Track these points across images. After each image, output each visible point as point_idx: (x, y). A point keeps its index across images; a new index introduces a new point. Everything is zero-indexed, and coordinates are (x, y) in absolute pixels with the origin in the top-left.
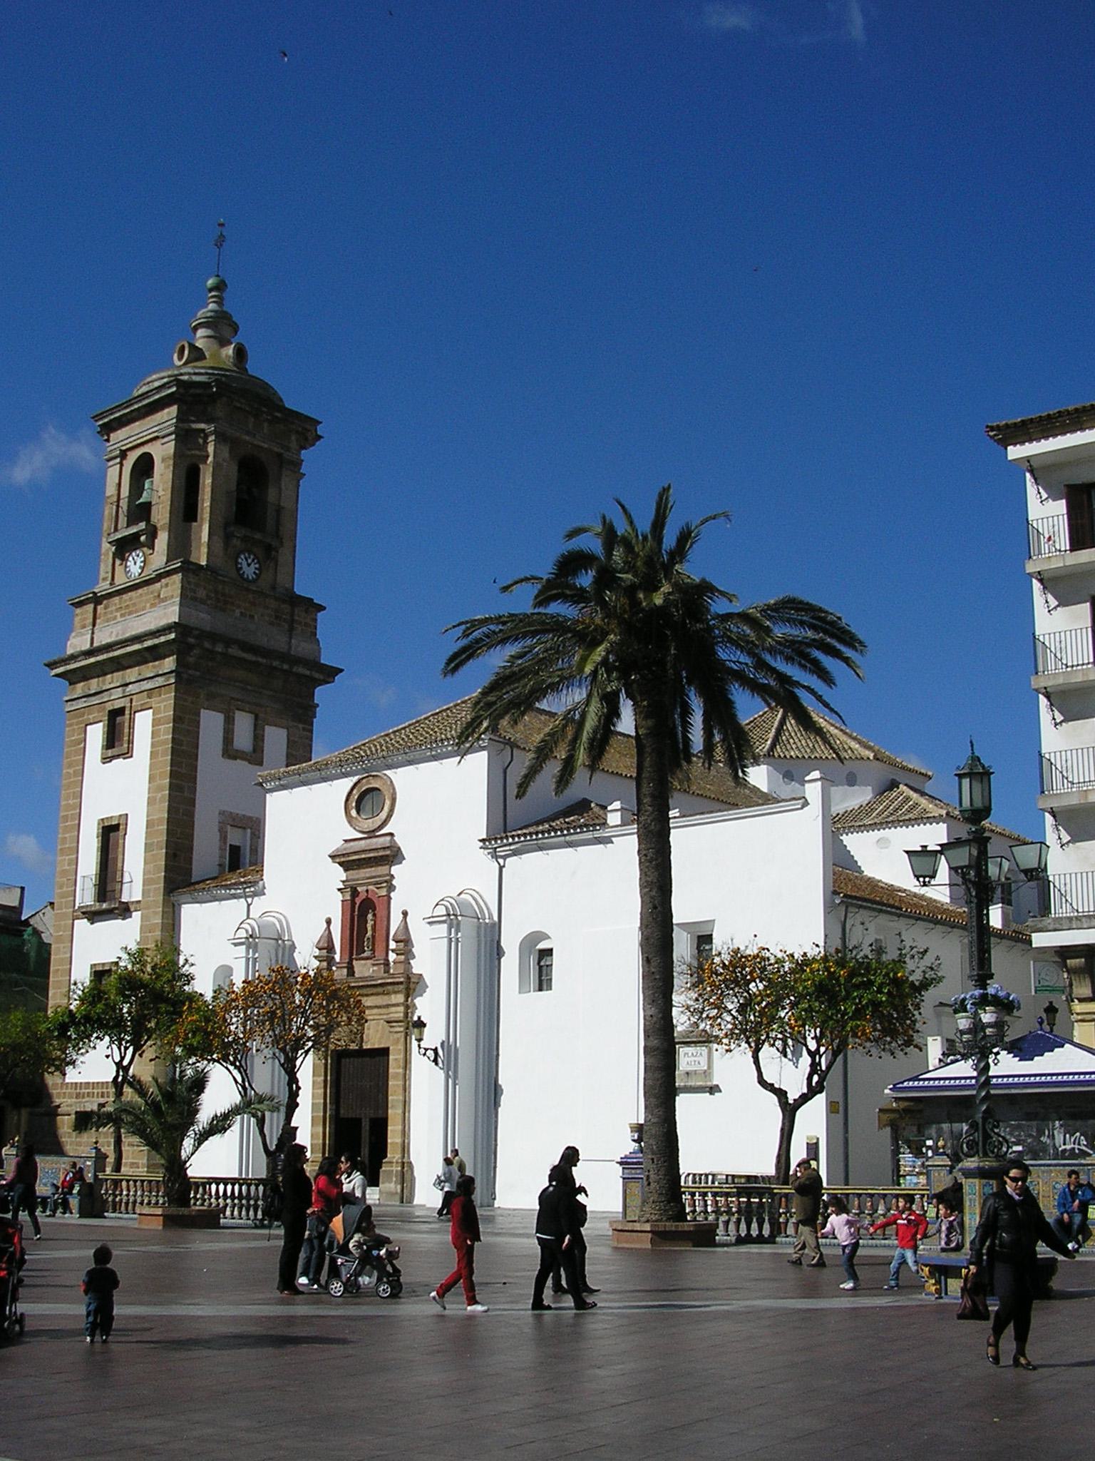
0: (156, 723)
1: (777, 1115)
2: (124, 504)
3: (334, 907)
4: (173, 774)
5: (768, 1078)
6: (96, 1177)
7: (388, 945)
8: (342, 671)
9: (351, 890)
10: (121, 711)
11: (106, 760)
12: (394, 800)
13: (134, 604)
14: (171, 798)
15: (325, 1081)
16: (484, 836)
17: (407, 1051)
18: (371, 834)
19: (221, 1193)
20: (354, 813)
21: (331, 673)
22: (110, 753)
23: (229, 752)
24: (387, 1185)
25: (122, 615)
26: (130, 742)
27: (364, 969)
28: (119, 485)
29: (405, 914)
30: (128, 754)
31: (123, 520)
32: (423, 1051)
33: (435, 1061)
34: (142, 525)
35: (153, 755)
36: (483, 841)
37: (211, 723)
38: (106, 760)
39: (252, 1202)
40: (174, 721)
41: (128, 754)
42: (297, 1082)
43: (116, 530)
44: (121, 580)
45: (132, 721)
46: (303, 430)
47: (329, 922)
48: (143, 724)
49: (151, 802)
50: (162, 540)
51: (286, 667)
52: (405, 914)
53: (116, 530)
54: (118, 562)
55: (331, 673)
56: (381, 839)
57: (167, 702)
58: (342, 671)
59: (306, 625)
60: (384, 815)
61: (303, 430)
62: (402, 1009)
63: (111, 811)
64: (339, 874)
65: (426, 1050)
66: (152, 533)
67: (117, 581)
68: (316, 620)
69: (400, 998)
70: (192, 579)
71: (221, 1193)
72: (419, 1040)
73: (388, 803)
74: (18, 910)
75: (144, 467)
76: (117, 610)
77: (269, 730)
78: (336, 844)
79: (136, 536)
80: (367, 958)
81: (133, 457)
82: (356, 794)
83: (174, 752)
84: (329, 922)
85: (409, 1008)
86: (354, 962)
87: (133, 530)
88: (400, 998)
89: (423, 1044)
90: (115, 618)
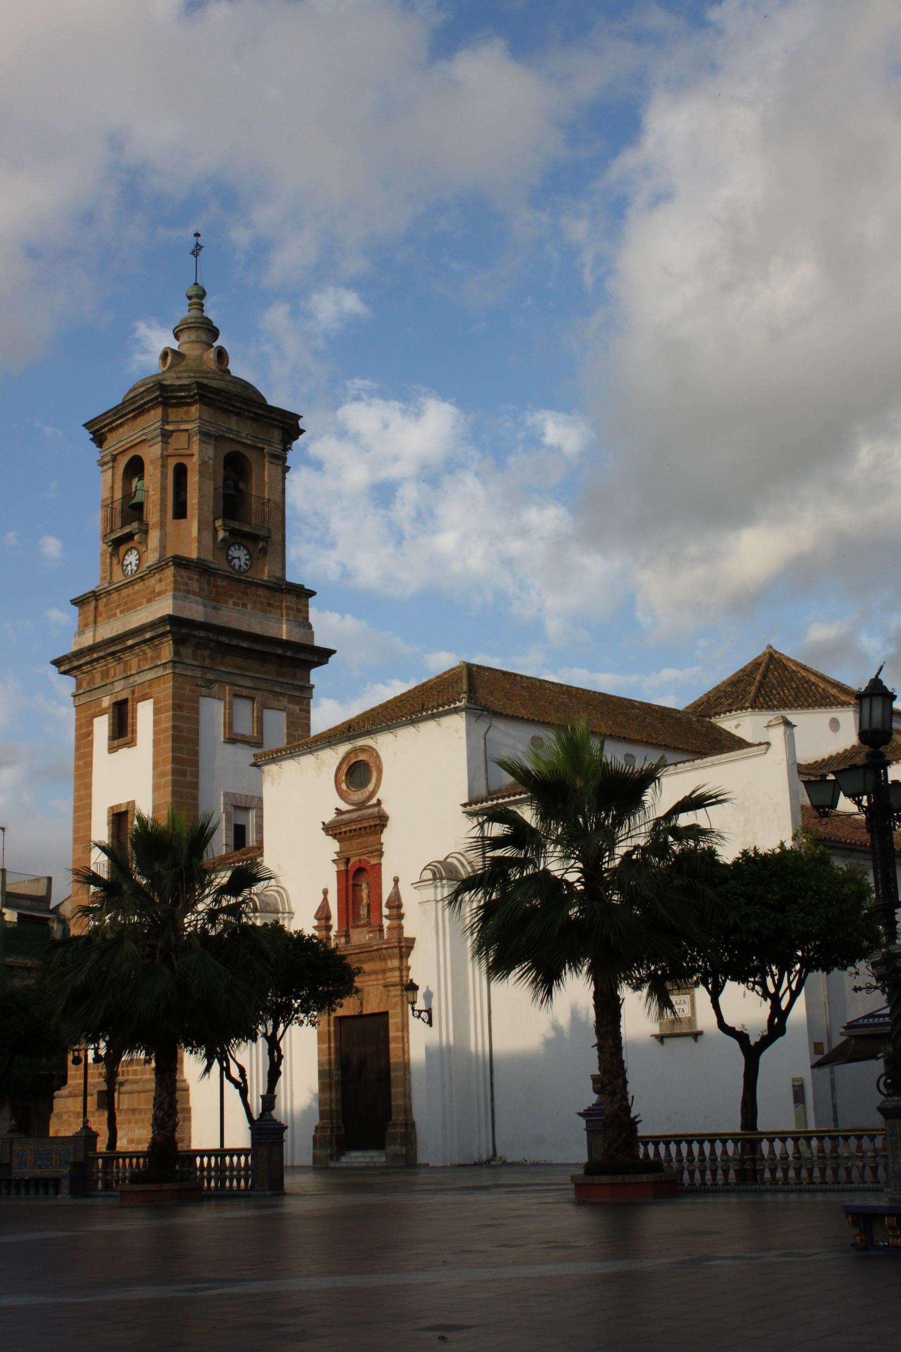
0: (157, 711)
1: (739, 1060)
2: (118, 506)
3: (328, 878)
4: (175, 760)
5: (729, 1021)
6: (86, 1155)
7: (381, 913)
8: (334, 652)
9: (343, 859)
10: (125, 701)
11: (112, 749)
12: (380, 771)
13: (132, 601)
14: (174, 783)
15: (329, 1048)
16: (466, 801)
17: (404, 1016)
18: (361, 805)
19: (205, 1164)
20: (344, 786)
21: (323, 655)
22: (116, 743)
23: (233, 739)
24: (392, 1147)
25: (121, 612)
26: (134, 731)
27: (360, 937)
28: (112, 488)
29: (396, 881)
30: (132, 743)
31: (118, 522)
32: (416, 1013)
33: (430, 1023)
34: (135, 525)
35: (156, 742)
36: (465, 805)
37: (213, 713)
38: (112, 749)
39: (205, 1173)
40: (174, 709)
41: (132, 743)
42: (279, 1050)
43: (112, 531)
44: (119, 578)
45: (135, 711)
46: (288, 427)
47: (325, 892)
48: (145, 715)
49: (156, 788)
50: (154, 537)
51: (279, 651)
52: (396, 881)
53: (112, 531)
54: (115, 561)
55: (323, 655)
56: (370, 811)
57: (166, 689)
58: (334, 652)
59: (299, 610)
60: (371, 787)
61: (288, 427)
62: (397, 973)
63: (120, 799)
64: (334, 846)
65: (420, 1012)
66: (145, 531)
67: (115, 580)
68: (307, 606)
69: (395, 963)
70: (184, 573)
71: (205, 1164)
72: (413, 1003)
73: (375, 775)
74: (47, 898)
75: (135, 468)
76: (117, 607)
77: (268, 715)
78: (330, 816)
79: (129, 537)
80: (364, 926)
81: (123, 462)
82: (345, 769)
83: (175, 739)
84: (325, 892)
85: (404, 969)
86: (351, 931)
87: (127, 530)
88: (395, 963)
89: (417, 1007)
90: (115, 615)
